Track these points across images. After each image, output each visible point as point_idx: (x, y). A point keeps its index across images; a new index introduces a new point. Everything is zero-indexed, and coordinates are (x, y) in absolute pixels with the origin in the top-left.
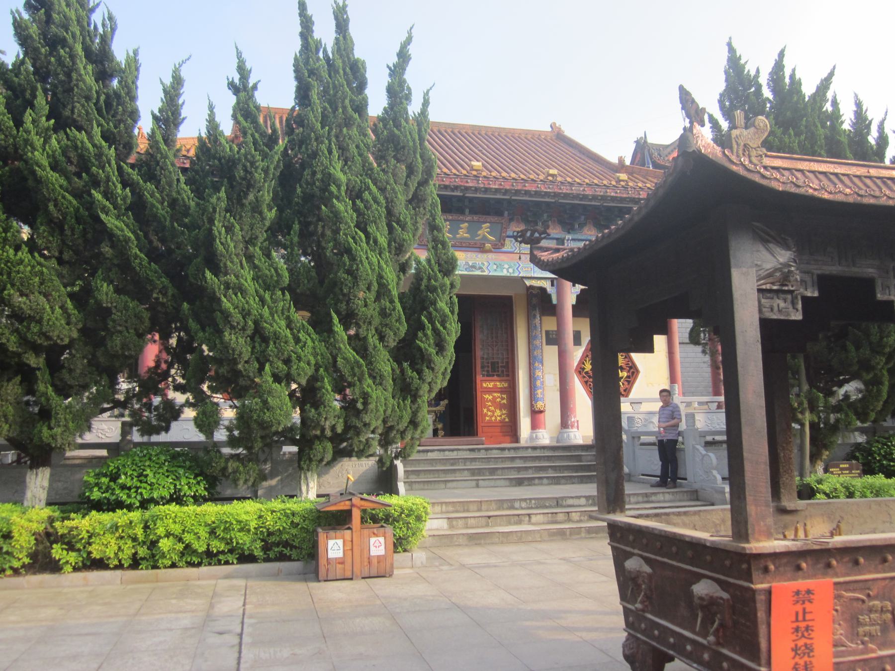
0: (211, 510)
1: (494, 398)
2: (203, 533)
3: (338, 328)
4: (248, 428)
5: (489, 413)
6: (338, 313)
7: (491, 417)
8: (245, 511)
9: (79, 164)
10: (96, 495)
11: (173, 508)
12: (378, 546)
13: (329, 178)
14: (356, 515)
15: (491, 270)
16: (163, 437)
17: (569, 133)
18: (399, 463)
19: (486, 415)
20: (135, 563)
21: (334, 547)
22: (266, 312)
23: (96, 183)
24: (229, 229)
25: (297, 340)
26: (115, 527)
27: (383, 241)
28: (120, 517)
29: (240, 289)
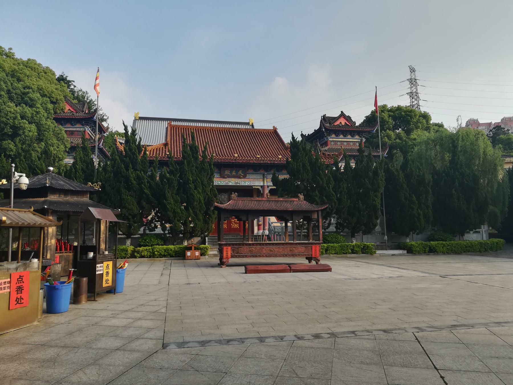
0: (165, 247)
2: (163, 251)
3: (191, 210)
4: (172, 230)
6: (191, 207)
8: (171, 247)
9: (139, 178)
10: (142, 243)
11: (158, 246)
12: (197, 253)
13: (189, 179)
14: (193, 247)
15: (243, 184)
16: (154, 232)
17: (278, 131)
18: (207, 238)
20: (150, 257)
21: (189, 254)
22: (176, 208)
23: (142, 183)
24: (169, 192)
25: (182, 213)
26: (147, 249)
27: (200, 191)
28: (147, 248)
29: (171, 203)
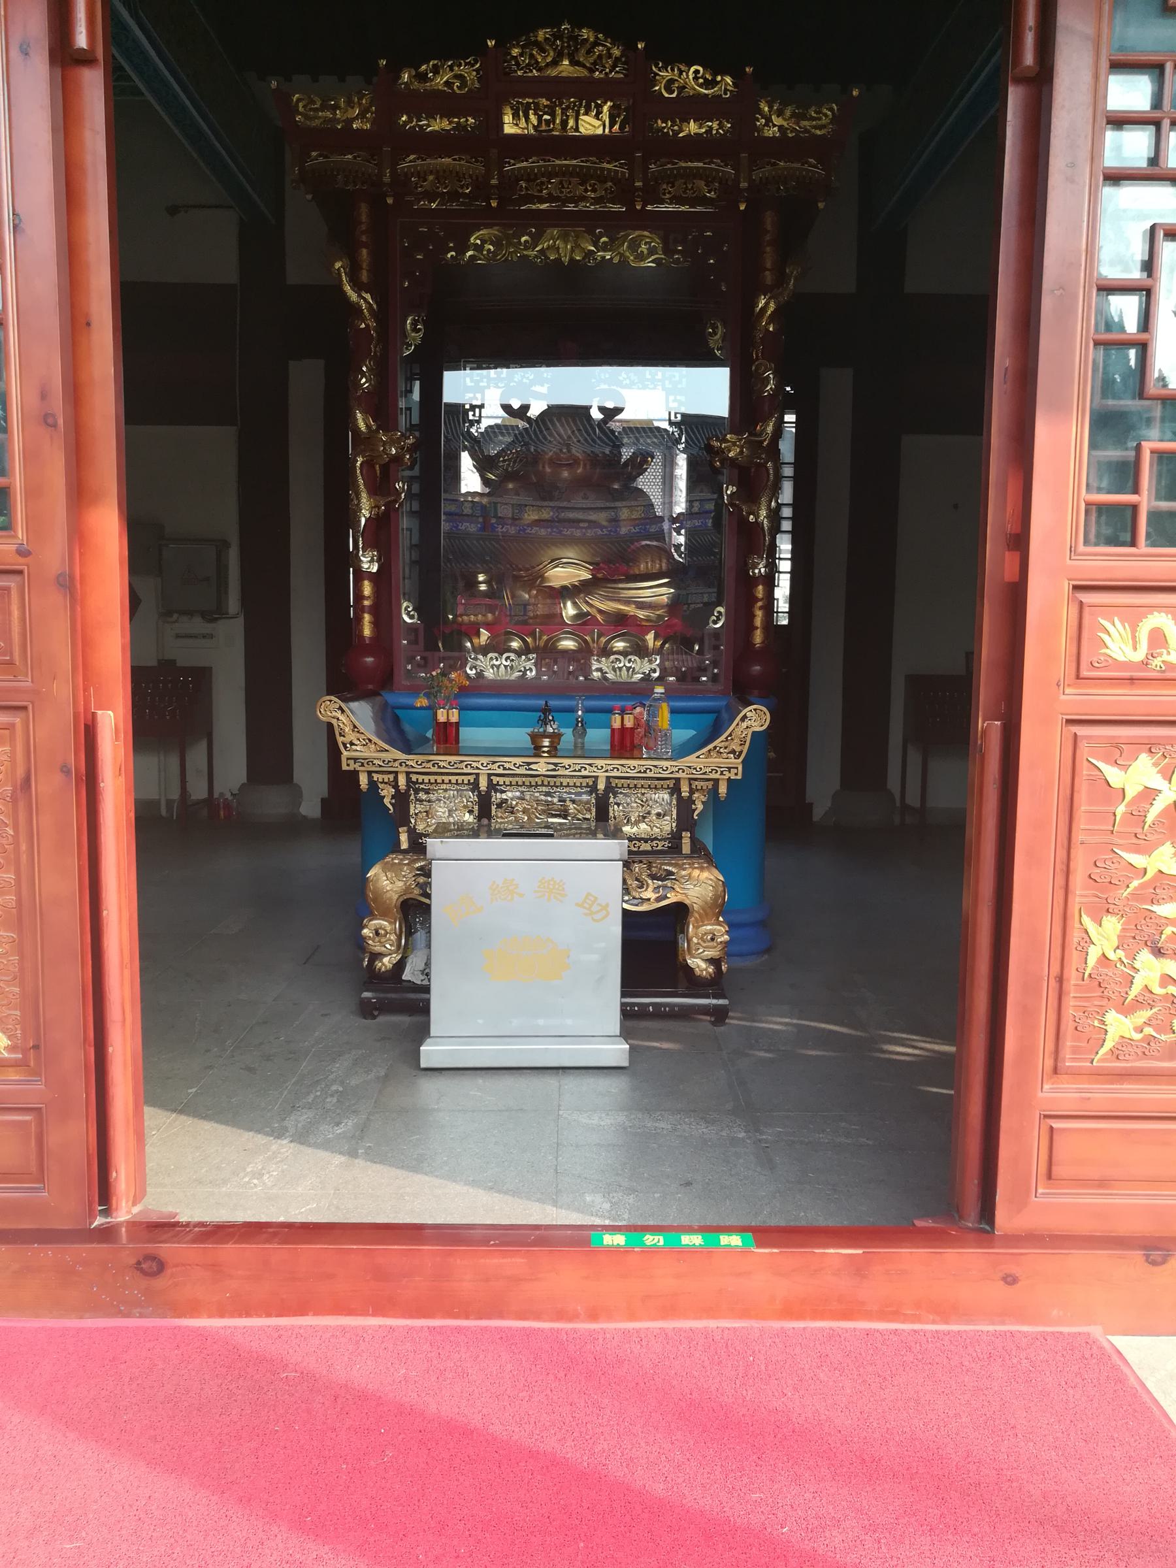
19: (1111, 988)
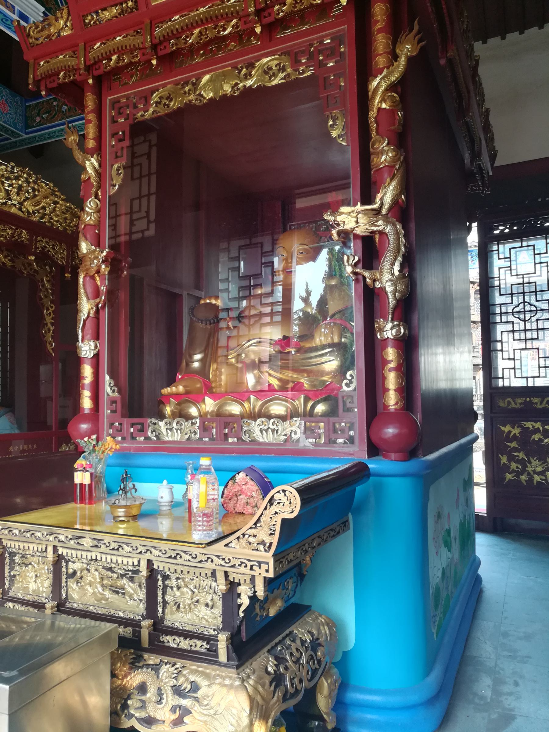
1: (527, 433)
5: (514, 466)
7: (518, 474)
